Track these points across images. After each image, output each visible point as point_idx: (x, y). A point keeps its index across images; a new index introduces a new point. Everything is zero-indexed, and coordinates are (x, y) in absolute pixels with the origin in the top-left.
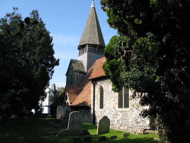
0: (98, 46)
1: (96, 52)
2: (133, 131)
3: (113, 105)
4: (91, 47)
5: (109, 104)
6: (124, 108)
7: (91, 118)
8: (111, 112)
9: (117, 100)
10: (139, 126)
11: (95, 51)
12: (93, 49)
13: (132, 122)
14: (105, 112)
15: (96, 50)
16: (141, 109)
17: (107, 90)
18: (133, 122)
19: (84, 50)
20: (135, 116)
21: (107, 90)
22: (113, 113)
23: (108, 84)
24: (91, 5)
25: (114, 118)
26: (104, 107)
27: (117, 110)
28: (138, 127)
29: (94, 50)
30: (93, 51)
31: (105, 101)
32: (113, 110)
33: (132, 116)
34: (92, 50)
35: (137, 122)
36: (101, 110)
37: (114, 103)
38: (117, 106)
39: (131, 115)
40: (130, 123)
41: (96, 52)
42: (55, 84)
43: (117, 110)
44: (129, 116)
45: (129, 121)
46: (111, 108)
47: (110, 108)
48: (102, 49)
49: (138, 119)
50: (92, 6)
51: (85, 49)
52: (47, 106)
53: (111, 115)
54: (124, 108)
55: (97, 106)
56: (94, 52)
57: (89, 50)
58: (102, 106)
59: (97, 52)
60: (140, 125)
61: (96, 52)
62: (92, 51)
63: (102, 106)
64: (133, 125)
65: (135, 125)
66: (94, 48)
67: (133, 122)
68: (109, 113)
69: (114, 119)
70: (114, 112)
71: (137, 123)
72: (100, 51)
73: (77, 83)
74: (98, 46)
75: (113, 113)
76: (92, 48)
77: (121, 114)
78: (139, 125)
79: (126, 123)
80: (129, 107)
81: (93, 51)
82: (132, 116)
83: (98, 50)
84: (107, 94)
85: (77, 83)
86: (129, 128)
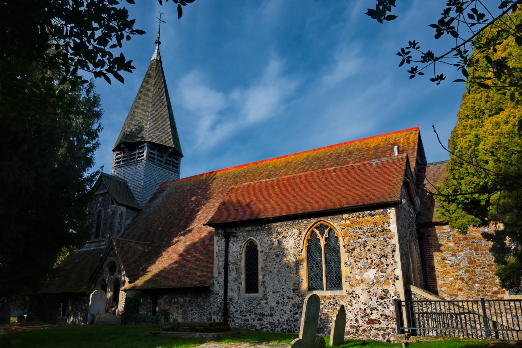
4: (154, 149)
5: (279, 281)
6: (327, 289)
11: (162, 161)
12: (158, 156)
13: (354, 320)
14: (263, 302)
15: (164, 159)
20: (363, 308)
24: (153, 54)
28: (375, 331)
29: (159, 158)
30: (158, 160)
32: (291, 295)
33: (353, 308)
34: (156, 157)
39: (351, 305)
41: (164, 162)
48: (174, 158)
50: (154, 57)
53: (285, 308)
54: (327, 289)
55: (235, 288)
56: (158, 162)
57: (150, 157)
60: (381, 326)
61: (164, 162)
62: (156, 161)
64: (357, 328)
65: (363, 328)
66: (159, 154)
67: (357, 321)
68: (278, 303)
71: (372, 322)
72: (170, 161)
75: (293, 302)
78: (377, 326)
80: (247, 295)
81: (158, 160)
82: (353, 308)
84: (269, 259)
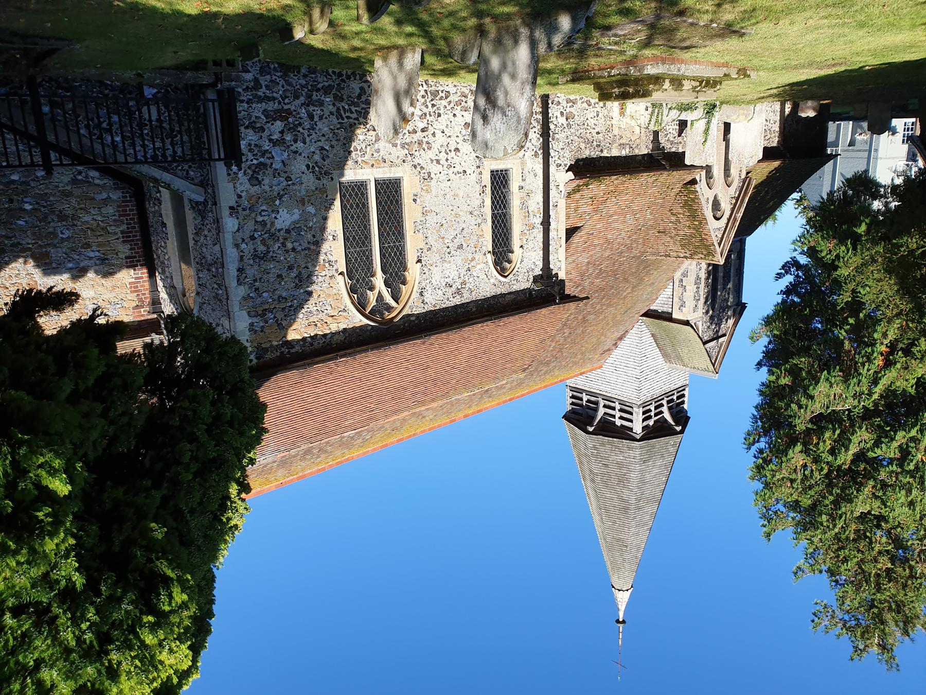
0: (591, 429)
1: (602, 403)
2: (305, 76)
3: (433, 189)
5: (456, 195)
7: (562, 120)
8: (443, 156)
9: (410, 214)
10: (274, 99)
12: (614, 416)
13: (316, 119)
16: (266, 181)
17: (473, 259)
18: (311, 117)
19: (656, 415)
20: (300, 145)
21: (470, 257)
22: (431, 154)
23: (464, 283)
25: (423, 130)
26: (487, 179)
27: (407, 167)
30: (614, 409)
31: (482, 205)
32: (434, 169)
33: (320, 144)
34: (618, 414)
35: (282, 119)
36: (499, 166)
37: (427, 200)
38: (408, 190)
39: (322, 149)
40: (327, 113)
42: (893, 134)
43: (407, 167)
44: (334, 143)
45: (334, 119)
46: (443, 177)
47: (452, 176)
49: (282, 132)
51: (650, 417)
52: (866, 171)
55: (529, 178)
56: (612, 405)
58: (500, 180)
59: (597, 403)
63: (500, 180)
65: (298, 102)
67: (311, 117)
68: (457, 150)
69: (421, 125)
70: (423, 158)
71: (281, 114)
73: (685, 275)
74: (591, 429)
75: (431, 154)
76: (619, 422)
77: (382, 153)
78: (271, 106)
79: (353, 109)
80: (398, 175)
81: (614, 409)
82: (320, 144)
83: (596, 410)
85: (685, 275)
86: (330, 88)
